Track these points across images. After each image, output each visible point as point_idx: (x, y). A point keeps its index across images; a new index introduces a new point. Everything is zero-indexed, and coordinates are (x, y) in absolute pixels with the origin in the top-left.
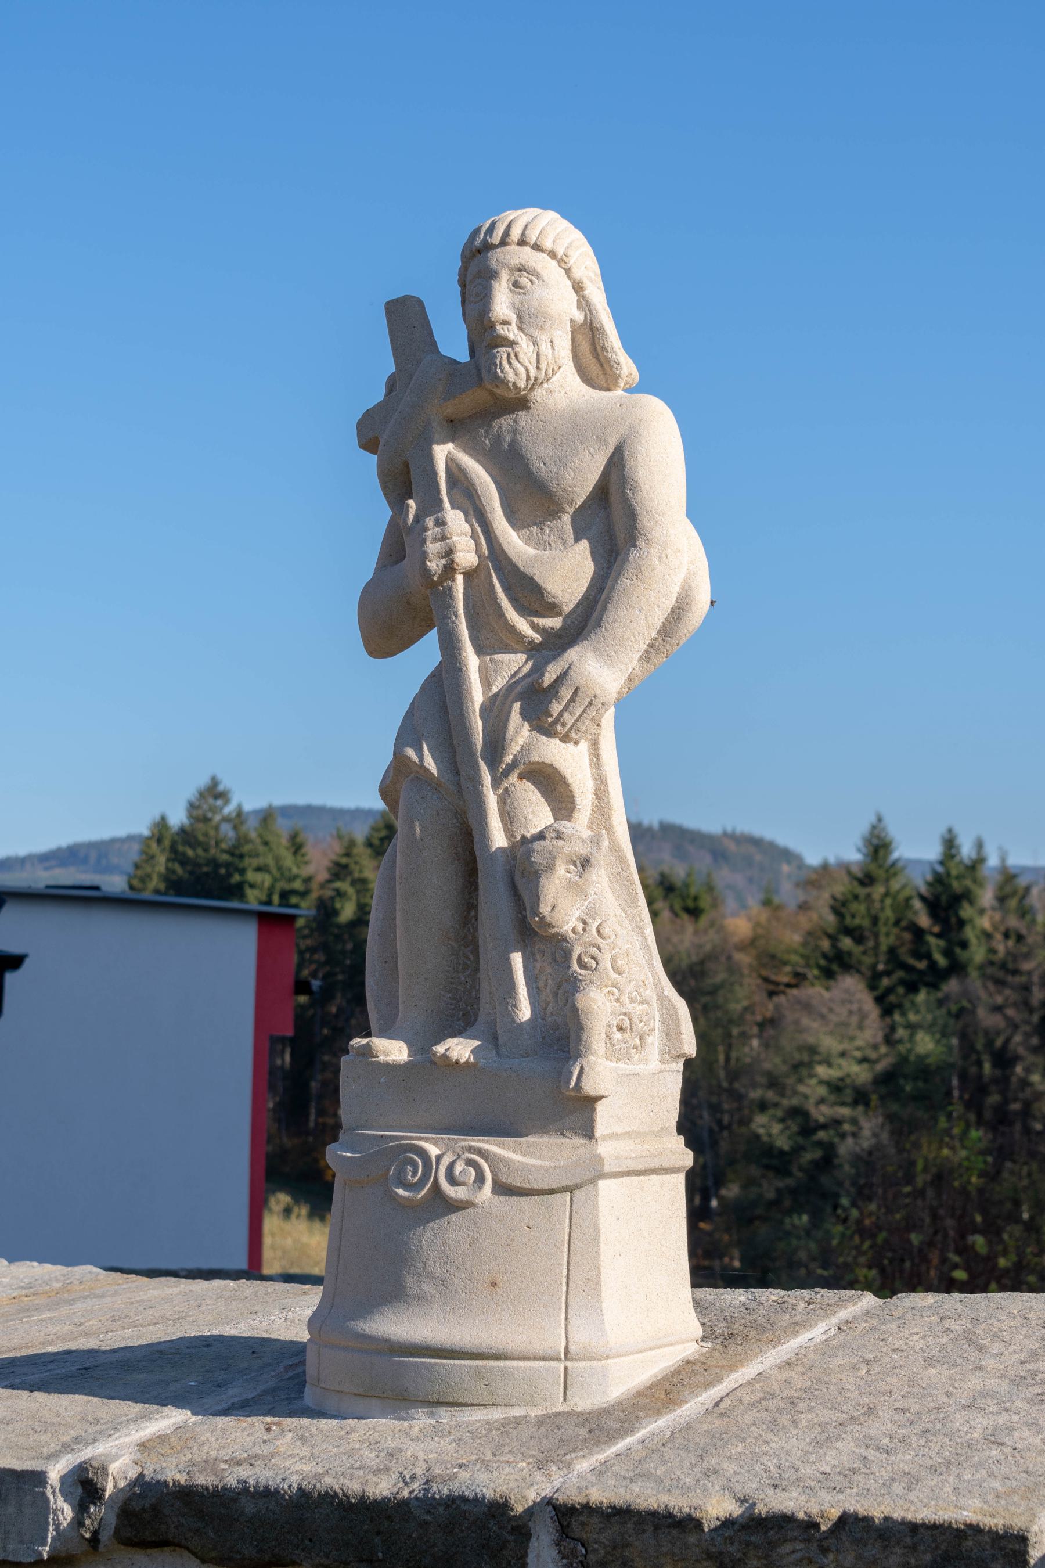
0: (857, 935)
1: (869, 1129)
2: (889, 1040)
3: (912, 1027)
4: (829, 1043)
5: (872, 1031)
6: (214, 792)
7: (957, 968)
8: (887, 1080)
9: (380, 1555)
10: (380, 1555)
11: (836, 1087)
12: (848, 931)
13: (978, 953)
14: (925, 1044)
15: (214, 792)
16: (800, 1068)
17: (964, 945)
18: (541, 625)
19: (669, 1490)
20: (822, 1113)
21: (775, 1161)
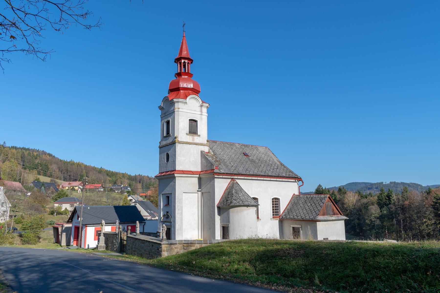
0: (380, 200)
1: (378, 222)
2: (381, 212)
3: (383, 210)
4: (374, 212)
5: (379, 210)
6: (320, 186)
7: (390, 204)
8: (381, 216)
9: (386, 290)
10: (386, 290)
11: (375, 217)
12: (379, 200)
13: (393, 202)
14: (385, 212)
15: (320, 186)
16: (371, 215)
17: (391, 201)
18: (8, 185)
19: (7, 155)
20: (373, 220)
21: (369, 225)
